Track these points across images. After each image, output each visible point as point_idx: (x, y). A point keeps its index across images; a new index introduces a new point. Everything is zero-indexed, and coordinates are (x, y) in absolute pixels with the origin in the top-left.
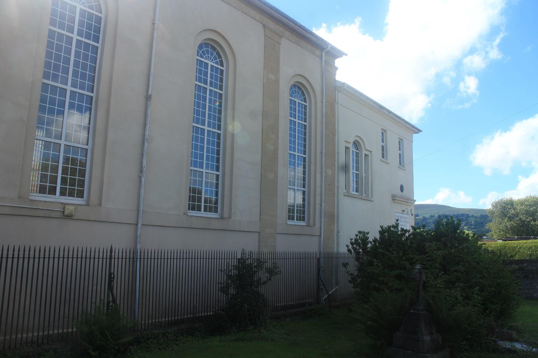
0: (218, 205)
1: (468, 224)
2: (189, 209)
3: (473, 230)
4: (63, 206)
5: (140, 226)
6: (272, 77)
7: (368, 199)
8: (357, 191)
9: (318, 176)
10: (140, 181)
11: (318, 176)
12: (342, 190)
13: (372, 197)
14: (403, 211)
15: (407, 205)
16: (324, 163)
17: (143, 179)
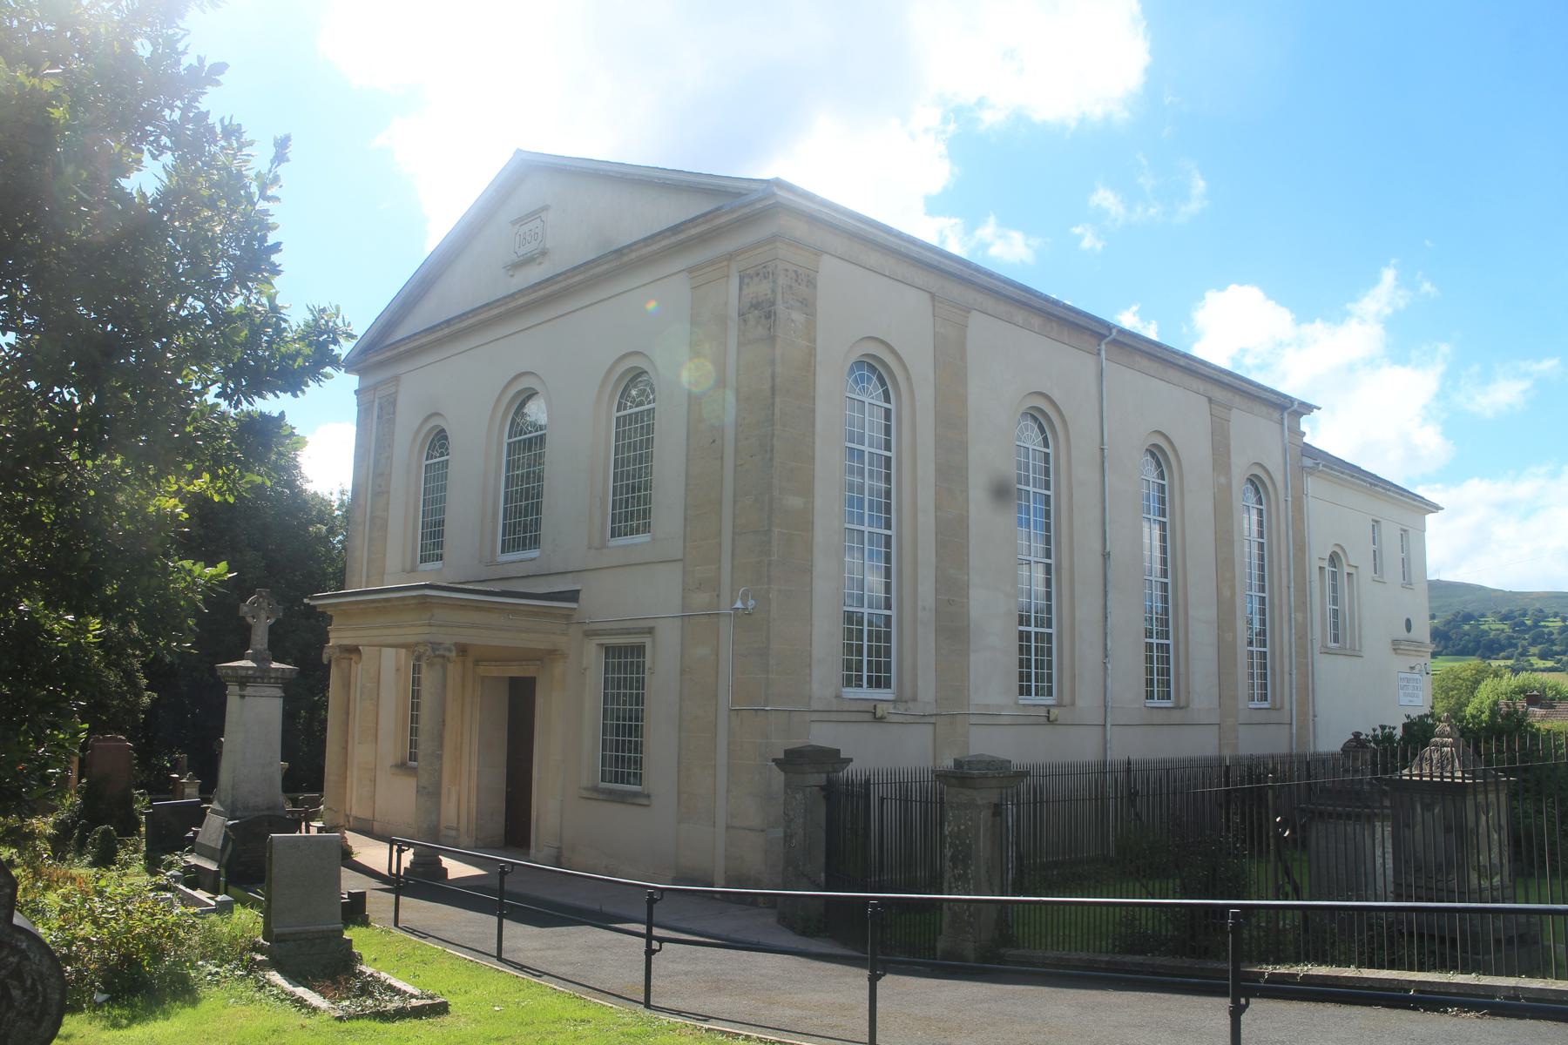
0: (891, 628)
1: (1539, 640)
2: (1147, 698)
3: (1559, 657)
4: (1046, 709)
5: (1108, 727)
6: (1223, 480)
7: (1355, 654)
8: (1336, 640)
9: (1285, 626)
10: (1106, 668)
11: (1285, 626)
12: (1317, 646)
13: (1360, 651)
14: (1412, 668)
15: (1418, 656)
16: (1293, 604)
17: (1109, 666)
